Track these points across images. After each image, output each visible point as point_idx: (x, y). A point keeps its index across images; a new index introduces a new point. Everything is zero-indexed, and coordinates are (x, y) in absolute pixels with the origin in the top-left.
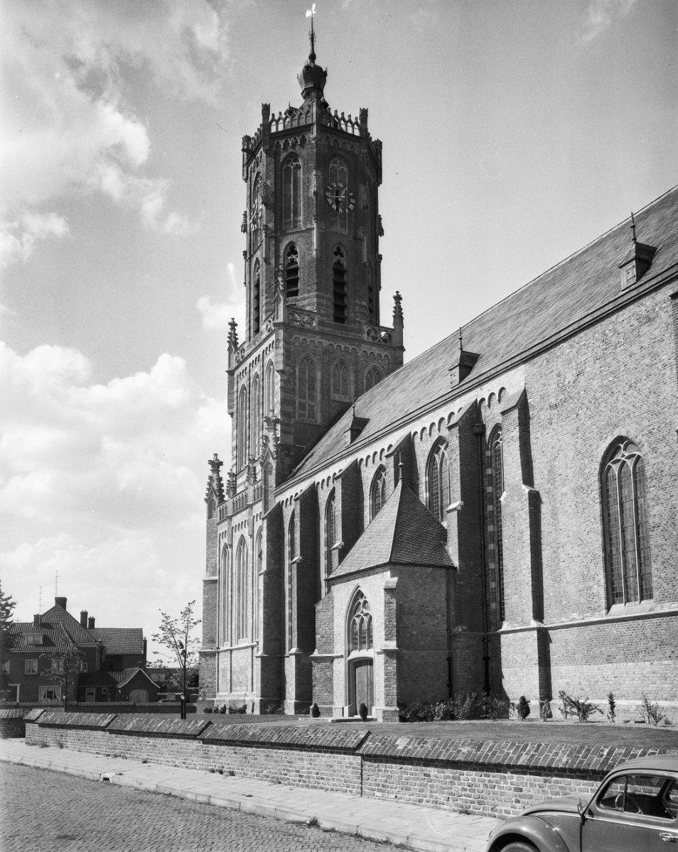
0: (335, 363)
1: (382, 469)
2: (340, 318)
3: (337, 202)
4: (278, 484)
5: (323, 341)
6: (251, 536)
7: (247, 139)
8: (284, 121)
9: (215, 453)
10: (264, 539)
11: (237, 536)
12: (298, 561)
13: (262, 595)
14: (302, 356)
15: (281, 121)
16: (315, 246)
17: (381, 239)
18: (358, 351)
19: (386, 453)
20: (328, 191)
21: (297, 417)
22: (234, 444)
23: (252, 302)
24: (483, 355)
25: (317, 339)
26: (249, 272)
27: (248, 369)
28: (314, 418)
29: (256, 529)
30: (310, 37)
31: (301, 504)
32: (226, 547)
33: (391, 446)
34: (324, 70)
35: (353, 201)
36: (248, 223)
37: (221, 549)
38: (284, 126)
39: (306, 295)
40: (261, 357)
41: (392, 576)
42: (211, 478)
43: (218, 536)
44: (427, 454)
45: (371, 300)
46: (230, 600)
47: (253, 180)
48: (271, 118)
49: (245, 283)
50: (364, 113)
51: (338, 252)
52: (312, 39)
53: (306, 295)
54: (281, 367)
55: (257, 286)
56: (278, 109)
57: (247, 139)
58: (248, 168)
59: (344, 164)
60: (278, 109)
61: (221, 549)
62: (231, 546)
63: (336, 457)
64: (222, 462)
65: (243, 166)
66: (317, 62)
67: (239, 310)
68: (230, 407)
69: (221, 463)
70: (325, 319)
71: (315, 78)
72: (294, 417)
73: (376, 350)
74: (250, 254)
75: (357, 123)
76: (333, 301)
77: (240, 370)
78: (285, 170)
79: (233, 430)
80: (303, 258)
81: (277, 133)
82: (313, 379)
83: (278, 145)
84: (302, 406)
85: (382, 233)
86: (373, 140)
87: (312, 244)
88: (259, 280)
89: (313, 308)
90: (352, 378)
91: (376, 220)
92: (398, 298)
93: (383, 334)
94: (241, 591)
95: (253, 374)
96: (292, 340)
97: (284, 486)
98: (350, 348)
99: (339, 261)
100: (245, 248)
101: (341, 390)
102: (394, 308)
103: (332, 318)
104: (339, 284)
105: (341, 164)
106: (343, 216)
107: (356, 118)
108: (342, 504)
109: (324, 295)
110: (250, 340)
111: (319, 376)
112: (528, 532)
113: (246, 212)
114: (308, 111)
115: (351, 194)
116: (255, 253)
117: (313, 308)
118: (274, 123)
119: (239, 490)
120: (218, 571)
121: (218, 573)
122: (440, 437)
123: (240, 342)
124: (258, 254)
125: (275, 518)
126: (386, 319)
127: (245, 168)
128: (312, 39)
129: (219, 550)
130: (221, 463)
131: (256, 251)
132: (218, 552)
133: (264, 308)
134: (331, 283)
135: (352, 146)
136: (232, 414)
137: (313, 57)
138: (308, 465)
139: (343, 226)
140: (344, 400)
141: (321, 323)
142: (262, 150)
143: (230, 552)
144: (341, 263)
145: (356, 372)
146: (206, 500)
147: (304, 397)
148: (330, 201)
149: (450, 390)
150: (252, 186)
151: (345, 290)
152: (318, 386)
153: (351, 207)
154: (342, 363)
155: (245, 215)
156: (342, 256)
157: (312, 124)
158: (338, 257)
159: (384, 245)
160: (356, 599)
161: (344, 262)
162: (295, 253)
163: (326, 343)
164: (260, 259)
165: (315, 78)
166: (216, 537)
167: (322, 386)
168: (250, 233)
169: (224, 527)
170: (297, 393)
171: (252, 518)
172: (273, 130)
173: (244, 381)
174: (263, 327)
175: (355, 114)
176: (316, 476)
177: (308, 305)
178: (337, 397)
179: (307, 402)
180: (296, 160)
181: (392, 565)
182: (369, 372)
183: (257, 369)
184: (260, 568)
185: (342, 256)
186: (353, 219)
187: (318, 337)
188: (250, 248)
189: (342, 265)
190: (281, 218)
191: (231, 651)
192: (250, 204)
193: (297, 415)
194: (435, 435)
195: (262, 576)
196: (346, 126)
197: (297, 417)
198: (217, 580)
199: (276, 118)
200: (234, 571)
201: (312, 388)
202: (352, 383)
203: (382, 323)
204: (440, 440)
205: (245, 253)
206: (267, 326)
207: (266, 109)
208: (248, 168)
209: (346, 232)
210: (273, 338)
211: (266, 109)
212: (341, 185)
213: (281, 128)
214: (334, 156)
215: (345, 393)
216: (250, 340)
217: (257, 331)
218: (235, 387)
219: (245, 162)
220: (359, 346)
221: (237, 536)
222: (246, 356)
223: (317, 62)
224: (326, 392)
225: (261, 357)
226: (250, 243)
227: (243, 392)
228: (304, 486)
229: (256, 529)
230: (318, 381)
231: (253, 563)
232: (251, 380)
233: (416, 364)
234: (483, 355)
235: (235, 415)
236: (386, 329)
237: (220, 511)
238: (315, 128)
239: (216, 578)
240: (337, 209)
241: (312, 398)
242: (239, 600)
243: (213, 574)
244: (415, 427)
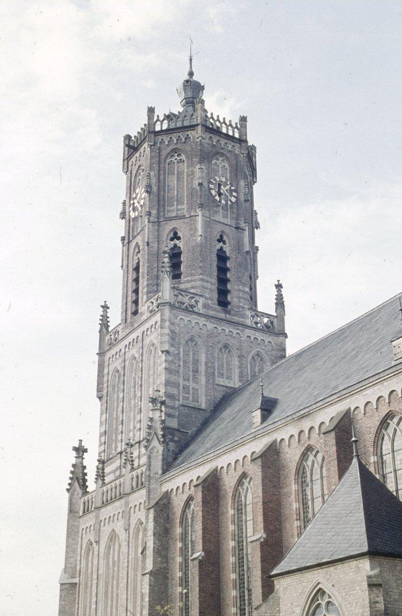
0: (220, 346)
1: (190, 499)
2: (223, 303)
3: (220, 194)
4: (165, 471)
5: (208, 324)
6: (126, 530)
7: (128, 137)
9: (80, 439)
10: (150, 533)
11: (106, 530)
12: (201, 558)
13: (147, 599)
14: (187, 337)
18: (242, 335)
19: (195, 483)
20: (212, 183)
21: (181, 400)
22: (103, 429)
23: (130, 285)
25: (202, 321)
26: (126, 256)
27: (123, 351)
28: (198, 402)
30: (189, 58)
31: (203, 492)
33: (199, 477)
34: (202, 85)
35: (235, 194)
36: (127, 211)
37: (84, 547)
39: (189, 278)
40: (140, 338)
41: (372, 569)
43: (81, 531)
44: (374, 431)
45: (251, 289)
46: (94, 606)
47: (134, 173)
48: (155, 119)
49: (122, 266)
50: (243, 119)
51: (221, 240)
52: (191, 60)
53: (189, 278)
55: (137, 269)
56: (160, 113)
57: (128, 137)
58: (128, 162)
59: (225, 161)
60: (160, 113)
61: (84, 547)
62: (97, 542)
63: (247, 438)
64: (87, 449)
65: (124, 161)
66: (195, 78)
70: (210, 302)
72: (179, 400)
73: (259, 336)
74: (129, 239)
75: (237, 127)
76: (217, 285)
77: (113, 352)
78: (169, 164)
79: (101, 414)
80: (186, 244)
81: (162, 131)
82: (196, 362)
83: (162, 142)
84: (186, 388)
86: (249, 144)
87: (196, 230)
88: (138, 263)
90: (237, 363)
91: (253, 213)
94: (110, 595)
95: (129, 355)
96: (177, 321)
97: (176, 472)
98: (235, 331)
99: (222, 248)
101: (225, 375)
102: (276, 295)
103: (216, 302)
104: (222, 270)
105: (223, 160)
106: (225, 208)
107: (236, 123)
108: (263, 489)
109: (209, 279)
110: (126, 322)
111: (203, 358)
112: (342, 556)
113: (125, 201)
115: (233, 188)
116: (134, 237)
118: (159, 123)
119: (107, 480)
120: (78, 573)
121: (78, 576)
122: (390, 411)
123: (112, 326)
124: (139, 239)
125: (162, 508)
126: (266, 303)
127: (126, 162)
128: (191, 60)
129: (81, 549)
131: (135, 237)
132: (79, 550)
133: (145, 290)
134: (215, 269)
135: (233, 146)
136: (100, 398)
137: (191, 74)
138: (178, 462)
139: (225, 216)
140: (229, 385)
141: (205, 306)
142: (146, 145)
143: (96, 549)
144: (224, 250)
145: (241, 357)
146: (68, 490)
147: (188, 380)
148: (213, 192)
149: (393, 363)
150: (133, 179)
151: (228, 276)
152: (202, 368)
153: (234, 200)
154: (226, 346)
155: (124, 203)
156: (224, 243)
157: (197, 125)
158: (221, 244)
160: (314, 599)
161: (227, 249)
163: (210, 326)
164: (140, 244)
166: (78, 532)
167: (207, 368)
168: (129, 220)
169: (88, 521)
170: (181, 374)
171: (128, 510)
173: (117, 364)
174: (143, 308)
175: (235, 120)
176: (220, 460)
177: (192, 288)
178: (220, 381)
179: (191, 384)
181: (373, 553)
182: (253, 357)
183: (134, 352)
184: (144, 568)
185: (224, 243)
186: (235, 211)
187: (203, 319)
188: (129, 233)
189: (225, 252)
190: (164, 206)
192: (130, 193)
193: (181, 397)
194: (384, 410)
195: (148, 575)
197: (181, 400)
198: (76, 584)
200: (101, 571)
201: (196, 371)
202: (237, 368)
204: (244, 475)
205: (123, 239)
206: (149, 307)
207: (151, 111)
208: (128, 162)
209: (228, 221)
210: (157, 317)
211: (151, 111)
212: (224, 180)
213: (165, 127)
214: (218, 153)
215: (229, 378)
216: (126, 322)
217: (135, 313)
219: (126, 157)
220: (242, 331)
221: (106, 530)
222: (120, 338)
223: (195, 78)
224: (210, 375)
226: (129, 229)
227: (115, 376)
228: (203, 471)
229: (133, 522)
230: (203, 364)
231: (128, 562)
235: (105, 398)
237: (84, 503)
239: (76, 580)
240: (220, 201)
241: (195, 380)
242: (106, 608)
244: (356, 402)
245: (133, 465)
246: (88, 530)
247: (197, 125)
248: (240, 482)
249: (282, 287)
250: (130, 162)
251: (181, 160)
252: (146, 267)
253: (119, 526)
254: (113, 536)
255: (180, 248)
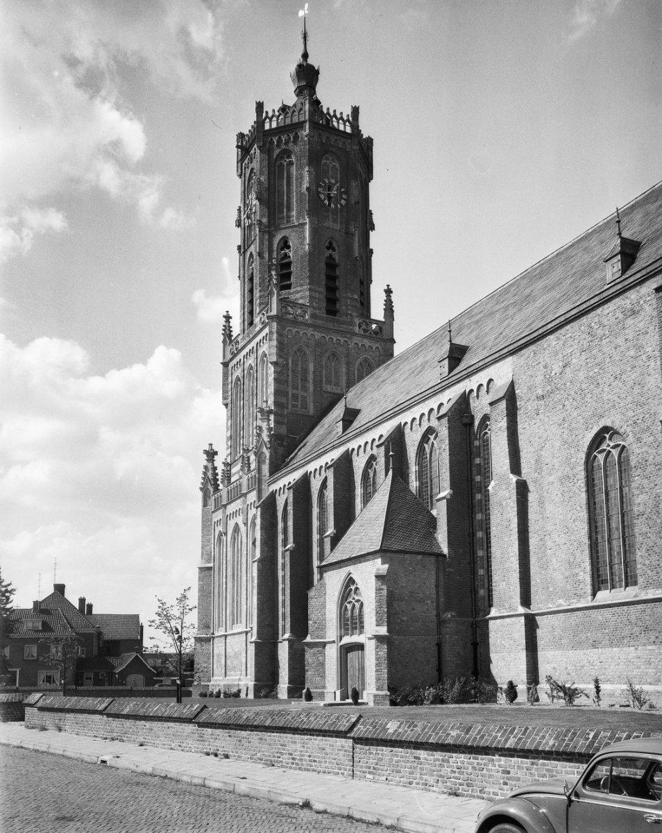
0: (327, 355)
1: (373, 458)
2: (332, 311)
3: (329, 198)
4: (272, 473)
5: (316, 333)
6: (245, 524)
7: (241, 136)
8: (278, 119)
9: (210, 443)
10: (258, 527)
11: (231, 524)
12: (291, 549)
13: (256, 581)
14: (295, 348)
15: (275, 119)
16: (307, 241)
17: (372, 234)
18: (349, 343)
19: (377, 443)
20: (321, 186)
21: (290, 407)
22: (229, 434)
23: (246, 295)
24: (472, 347)
25: (310, 331)
26: (243, 266)
27: (242, 360)
28: (306, 409)
29: (250, 517)
30: (303, 36)
31: (294, 493)
32: (220, 534)
33: (381, 436)
34: (316, 69)
35: (345, 197)
36: (242, 218)
37: (216, 537)
38: (278, 123)
39: (299, 289)
40: (255, 349)
42: (206, 467)
43: (213, 524)
44: (417, 444)
45: (362, 294)
46: (224, 586)
47: (247, 176)
48: (264, 115)
49: (239, 277)
50: (356, 111)
51: (330, 247)
52: (305, 38)
53: (299, 289)
54: (274, 359)
55: (251, 279)
56: (271, 107)
57: (241, 136)
58: (242, 164)
59: (335, 160)
60: (271, 107)
61: (216, 537)
62: (226, 534)
63: (328, 447)
64: (217, 452)
65: (237, 163)
66: (310, 61)
67: (233, 303)
68: (225, 398)
69: (216, 453)
70: (318, 311)
71: (307, 76)
72: (287, 408)
73: (367, 343)
74: (244, 248)
75: (348, 120)
76: (325, 294)
77: (234, 362)
78: (279, 166)
79: (228, 420)
80: (296, 252)
81: (271, 130)
82: (305, 371)
83: (272, 142)
84: (295, 397)
85: (373, 228)
86: (364, 137)
87: (304, 238)
88: (252, 273)
89: (306, 301)
90: (344, 370)
91: (368, 215)
92: (388, 292)
93: (374, 326)
94: (236, 578)
95: (247, 365)
96: (285, 332)
97: (278, 476)
98: (342, 340)
99: (331, 256)
100: (239, 242)
101: (333, 381)
102: (385, 301)
103: (324, 311)
104: (331, 278)
105: (333, 160)
106: (335, 212)
107: (348, 116)
108: (334, 493)
109: (317, 288)
110: (244, 333)
111: (311, 367)
113: (240, 207)
114: (301, 109)
115: (343, 190)
116: (249, 247)
117: (306, 301)
118: (268, 120)
119: (233, 479)
120: (212, 559)
121: (212, 560)
122: (430, 427)
123: (234, 334)
124: (252, 249)
125: (268, 507)
126: (377, 312)
127: (240, 164)
128: (305, 38)
129: (214, 538)
130: (216, 453)
132: (213, 540)
133: (258, 302)
134: (323, 277)
135: (344, 143)
136: (226, 405)
137: (305, 56)
138: (301, 454)
140: (336, 391)
142: (255, 146)
143: (225, 539)
144: (333, 257)
145: (348, 364)
146: (201, 489)
147: (297, 388)
148: (322, 197)
149: (439, 381)
150: (247, 182)
151: (337, 283)
152: (311, 377)
153: (343, 202)
154: (334, 355)
155: (239, 210)
156: (334, 250)
157: (305, 122)
158: (330, 251)
159: (375, 240)
160: (347, 586)
161: (336, 256)
162: (289, 247)
163: (318, 335)
164: (254, 253)
165: (307, 76)
166: (211, 525)
167: (314, 377)
168: (244, 227)
170: (290, 384)
171: (246, 507)
172: (267, 127)
173: (238, 373)
174: (257, 320)
175: (347, 112)
176: (309, 465)
177: (301, 298)
178: (329, 388)
179: (300, 393)
180: (289, 157)
181: (383, 552)
182: (361, 364)
183: (251, 361)
184: (253, 556)
185: (334, 250)
187: (311, 329)
188: (244, 242)
189: (334, 259)
190: (274, 213)
191: (226, 636)
192: (244, 200)
193: (290, 405)
194: (425, 425)
195: (256, 563)
196: (338, 123)
197: (290, 407)
198: (211, 568)
199: (270, 115)
200: (228, 558)
201: (305, 380)
202: (344, 374)
203: (373, 316)
204: (430, 430)
205: (239, 248)
206: (261, 319)
207: (260, 106)
208: (242, 164)
209: (337, 227)
210: (267, 330)
211: (260, 106)
212: (333, 181)
213: (274, 125)
214: (326, 152)
215: (337, 384)
216: (244, 333)
217: (251, 323)
218: (230, 378)
219: (239, 158)
220: (351, 338)
221: (231, 524)
222: (240, 348)
223: (310, 61)
224: (318, 383)
225: (255, 349)
226: (245, 237)
227: (237, 384)
228: (297, 475)
230: (311, 373)
231: (247, 550)
232: (246, 372)
233: (406, 356)
234: (472, 347)
235: (229, 405)
236: (377, 322)
238: (307, 125)
239: (211, 565)
241: (305, 389)
242: (233, 587)
243: (208, 561)
245: (250, 467)
246: (282, 491)
247: (305, 122)
248: (425, 438)
249: (392, 292)
250: (244, 164)
251: (290, 161)
252: (258, 279)
253: (240, 520)
254: (236, 529)
255: (289, 257)
